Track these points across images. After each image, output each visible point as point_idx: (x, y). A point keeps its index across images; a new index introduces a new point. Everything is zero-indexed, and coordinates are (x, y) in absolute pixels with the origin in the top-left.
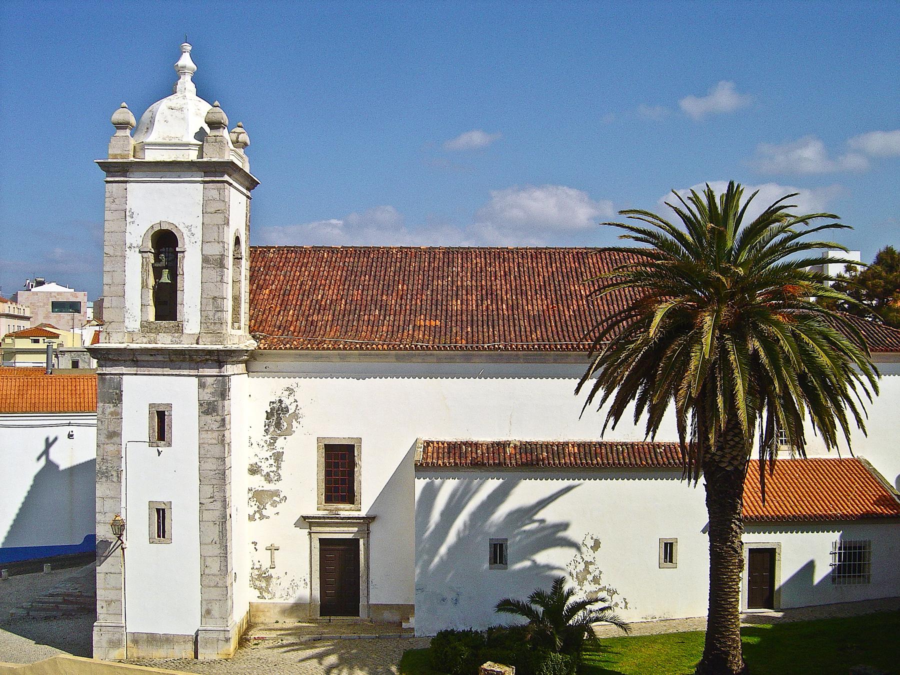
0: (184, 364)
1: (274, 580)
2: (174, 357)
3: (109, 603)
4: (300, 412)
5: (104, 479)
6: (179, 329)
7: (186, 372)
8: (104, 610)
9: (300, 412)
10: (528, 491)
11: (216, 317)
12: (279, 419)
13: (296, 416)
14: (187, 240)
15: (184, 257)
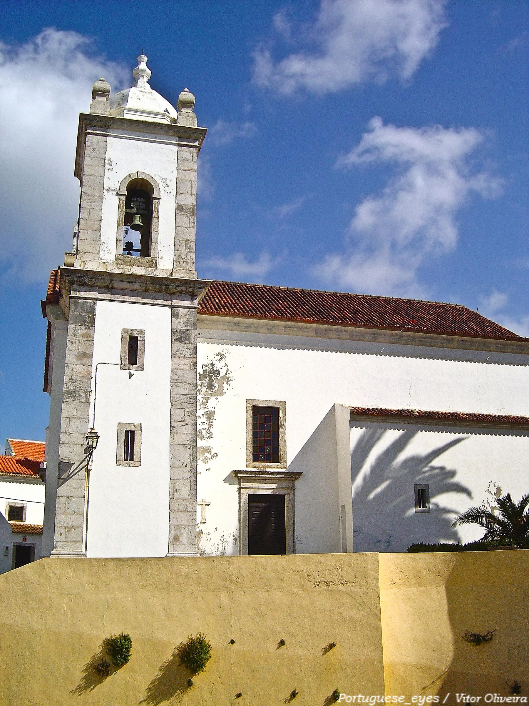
0: (158, 295)
1: (204, 536)
2: (150, 287)
3: (68, 529)
4: (231, 375)
5: (71, 399)
6: (153, 264)
7: (160, 302)
8: (63, 538)
9: (231, 375)
10: (424, 442)
11: (189, 257)
12: (211, 380)
13: (226, 378)
14: (162, 189)
15: (159, 204)
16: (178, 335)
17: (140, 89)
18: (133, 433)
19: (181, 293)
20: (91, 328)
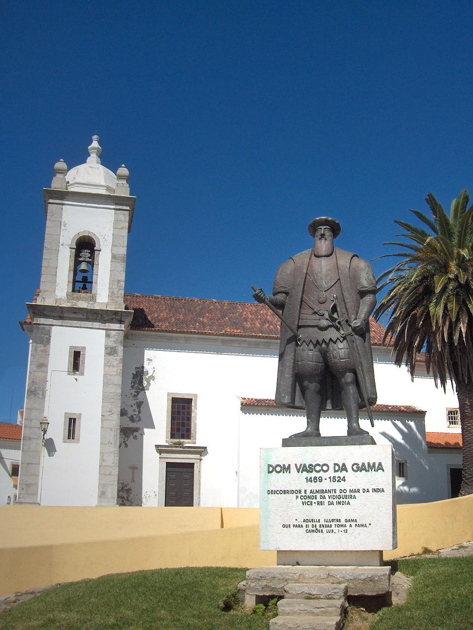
6: (93, 299)
13: (152, 377)
14: (101, 244)
16: (109, 350)
18: (75, 419)
19: (112, 320)
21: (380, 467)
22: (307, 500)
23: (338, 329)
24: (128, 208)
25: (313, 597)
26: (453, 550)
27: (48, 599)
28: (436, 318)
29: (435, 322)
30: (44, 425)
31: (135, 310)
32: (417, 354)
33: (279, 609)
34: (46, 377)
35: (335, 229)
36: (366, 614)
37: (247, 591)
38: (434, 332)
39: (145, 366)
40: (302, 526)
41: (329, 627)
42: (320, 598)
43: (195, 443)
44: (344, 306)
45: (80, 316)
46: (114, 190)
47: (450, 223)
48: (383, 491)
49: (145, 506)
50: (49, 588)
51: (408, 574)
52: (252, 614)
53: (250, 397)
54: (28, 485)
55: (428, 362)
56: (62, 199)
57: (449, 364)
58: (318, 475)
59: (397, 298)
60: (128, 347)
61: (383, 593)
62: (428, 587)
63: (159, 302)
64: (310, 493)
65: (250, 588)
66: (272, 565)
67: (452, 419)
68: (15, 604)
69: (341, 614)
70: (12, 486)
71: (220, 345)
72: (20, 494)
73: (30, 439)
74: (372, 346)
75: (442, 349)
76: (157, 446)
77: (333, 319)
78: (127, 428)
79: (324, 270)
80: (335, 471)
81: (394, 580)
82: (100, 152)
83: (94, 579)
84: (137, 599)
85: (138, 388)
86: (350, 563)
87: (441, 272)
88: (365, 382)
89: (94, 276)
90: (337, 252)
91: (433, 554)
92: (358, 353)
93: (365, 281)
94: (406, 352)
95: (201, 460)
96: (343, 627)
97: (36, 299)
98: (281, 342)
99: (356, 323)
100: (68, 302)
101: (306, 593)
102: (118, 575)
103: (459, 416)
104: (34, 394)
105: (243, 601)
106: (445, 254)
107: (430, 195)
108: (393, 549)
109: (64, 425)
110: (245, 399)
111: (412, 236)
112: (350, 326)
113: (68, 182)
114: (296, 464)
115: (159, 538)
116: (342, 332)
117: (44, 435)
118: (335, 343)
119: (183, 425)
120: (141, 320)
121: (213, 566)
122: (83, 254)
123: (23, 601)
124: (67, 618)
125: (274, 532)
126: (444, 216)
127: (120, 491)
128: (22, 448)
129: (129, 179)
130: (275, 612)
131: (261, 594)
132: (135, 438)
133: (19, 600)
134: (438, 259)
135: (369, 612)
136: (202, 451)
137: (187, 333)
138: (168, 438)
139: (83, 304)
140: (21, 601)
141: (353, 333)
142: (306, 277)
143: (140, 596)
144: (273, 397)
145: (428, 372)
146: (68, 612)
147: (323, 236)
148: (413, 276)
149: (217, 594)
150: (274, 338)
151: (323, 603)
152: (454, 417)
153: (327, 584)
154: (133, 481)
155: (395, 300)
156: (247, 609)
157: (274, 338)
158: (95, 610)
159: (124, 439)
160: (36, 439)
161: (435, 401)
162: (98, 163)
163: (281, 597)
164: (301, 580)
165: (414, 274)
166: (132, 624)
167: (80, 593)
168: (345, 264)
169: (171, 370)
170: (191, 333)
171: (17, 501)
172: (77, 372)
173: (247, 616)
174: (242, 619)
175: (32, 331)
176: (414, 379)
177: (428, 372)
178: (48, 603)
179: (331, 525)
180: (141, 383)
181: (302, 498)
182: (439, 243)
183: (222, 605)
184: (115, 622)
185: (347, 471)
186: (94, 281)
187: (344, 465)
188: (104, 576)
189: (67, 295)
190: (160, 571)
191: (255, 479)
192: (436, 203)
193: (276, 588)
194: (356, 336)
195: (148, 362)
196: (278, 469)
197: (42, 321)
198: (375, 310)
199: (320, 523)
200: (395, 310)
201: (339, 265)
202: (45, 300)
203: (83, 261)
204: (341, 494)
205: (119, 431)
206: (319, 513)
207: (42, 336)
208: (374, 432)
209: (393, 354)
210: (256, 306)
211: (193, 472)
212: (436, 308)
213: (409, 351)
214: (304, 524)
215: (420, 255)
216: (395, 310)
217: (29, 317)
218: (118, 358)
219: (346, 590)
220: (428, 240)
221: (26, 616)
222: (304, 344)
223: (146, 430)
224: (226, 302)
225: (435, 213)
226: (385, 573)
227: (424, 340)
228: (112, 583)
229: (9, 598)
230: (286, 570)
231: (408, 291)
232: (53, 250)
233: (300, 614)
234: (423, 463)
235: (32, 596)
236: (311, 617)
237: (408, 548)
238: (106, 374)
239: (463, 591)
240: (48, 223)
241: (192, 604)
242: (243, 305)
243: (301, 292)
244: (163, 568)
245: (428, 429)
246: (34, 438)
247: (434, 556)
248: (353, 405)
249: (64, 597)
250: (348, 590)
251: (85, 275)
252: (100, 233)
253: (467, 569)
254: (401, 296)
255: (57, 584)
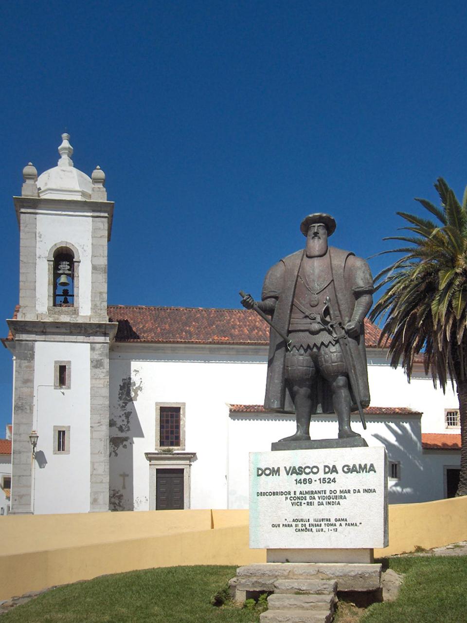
6: (76, 312)
13: (140, 388)
14: (80, 254)
16: (95, 363)
17: (62, 168)
18: (64, 432)
19: (96, 333)
20: (32, 361)
21: (372, 468)
22: (296, 501)
23: (330, 333)
24: (106, 215)
25: (302, 592)
26: (447, 549)
27: (44, 601)
28: (439, 316)
29: (437, 320)
30: (33, 439)
31: (119, 322)
32: (416, 355)
33: (269, 604)
34: (32, 392)
35: (329, 226)
36: (356, 609)
37: (238, 587)
38: (435, 332)
39: (132, 377)
40: (291, 526)
41: (319, 620)
42: (310, 593)
43: (184, 450)
44: (337, 309)
45: (63, 330)
46: (90, 195)
47: (462, 211)
48: (374, 491)
49: (136, 510)
50: (45, 590)
51: (399, 572)
52: (242, 608)
53: (239, 403)
54: (21, 497)
55: (427, 364)
56: (35, 208)
57: (450, 364)
58: (307, 477)
59: (396, 297)
60: (114, 359)
61: (374, 589)
62: (420, 584)
63: (143, 312)
64: (300, 494)
65: (240, 584)
66: (262, 563)
67: (451, 420)
68: (12, 608)
69: (330, 609)
70: (5, 497)
71: (208, 354)
72: (13, 505)
73: (20, 453)
74: (366, 349)
75: (443, 349)
76: (146, 454)
77: (325, 322)
78: (116, 438)
79: (317, 271)
80: (325, 473)
81: (385, 577)
82: (72, 152)
83: (89, 581)
84: (131, 597)
85: (125, 399)
86: (340, 561)
87: (447, 266)
88: (358, 386)
89: (75, 289)
90: (331, 251)
91: (426, 553)
92: (352, 356)
93: (361, 282)
94: (403, 353)
95: (190, 465)
96: (332, 621)
97: (16, 315)
98: (270, 349)
99: (350, 326)
100: (50, 317)
101: (296, 589)
102: (112, 575)
103: (458, 416)
104: (22, 409)
105: (234, 596)
106: (453, 246)
107: (441, 181)
108: (384, 547)
109: (54, 437)
110: (234, 405)
111: (415, 229)
112: (343, 328)
113: (39, 189)
114: (285, 467)
115: (151, 540)
116: (335, 335)
117: (34, 448)
118: (327, 346)
119: (172, 432)
120: (126, 332)
121: (204, 564)
122: (62, 266)
123: (20, 604)
124: (64, 617)
125: (263, 532)
126: (456, 203)
127: (112, 497)
128: (13, 462)
129: (105, 183)
130: (265, 606)
131: (252, 590)
132: (125, 446)
133: (16, 604)
134: (444, 252)
135: (359, 607)
136: (191, 457)
137: (174, 342)
138: (158, 446)
139: (65, 319)
140: (18, 605)
141: (347, 336)
142: (297, 279)
143: (134, 594)
144: (262, 403)
145: (427, 373)
146: (64, 612)
147: (316, 234)
148: (414, 272)
149: (208, 590)
150: (262, 344)
151: (313, 598)
152: (454, 418)
153: (317, 580)
154: (124, 487)
155: (394, 299)
156: (238, 604)
157: (262, 344)
158: (91, 609)
159: (114, 449)
160: (27, 452)
161: (433, 402)
162: (70, 165)
163: (271, 593)
164: (291, 576)
165: (415, 271)
166: (126, 620)
167: (76, 594)
168: (339, 263)
169: (158, 380)
170: (178, 342)
171: (10, 512)
172: (63, 387)
173: (238, 611)
174: (233, 614)
175: (14, 348)
176: (411, 380)
177: (427, 373)
178: (45, 605)
179: (321, 524)
180: (128, 393)
181: (291, 498)
182: (447, 234)
183: (213, 600)
184: (111, 619)
185: (337, 473)
186: (75, 294)
187: (334, 467)
188: (99, 577)
189: (49, 310)
190: (153, 571)
191: (244, 482)
192: (447, 189)
193: (266, 584)
194: (349, 339)
195: (135, 373)
196: (268, 472)
197: (24, 337)
198: (370, 311)
199: (309, 523)
200: (393, 310)
201: (333, 266)
202: (25, 316)
203: (62, 274)
204: (331, 495)
205: (108, 441)
206: (307, 512)
207: (26, 352)
208: (366, 435)
209: (389, 356)
210: (244, 313)
211: (183, 477)
212: (439, 306)
213: (406, 352)
214: (294, 524)
215: (424, 249)
216: (393, 310)
217: (10, 334)
218: (105, 371)
219: (336, 586)
220: (434, 232)
221: (23, 618)
222: (295, 348)
223: (135, 439)
224: (213, 309)
225: (445, 201)
226: (375, 570)
227: (424, 340)
228: (106, 584)
229: (6, 602)
230: (276, 567)
231: (408, 289)
232: (29, 263)
233: (290, 608)
234: (418, 464)
235: (30, 599)
236: (300, 611)
237: (401, 545)
238: (94, 387)
239: (459, 589)
240: (22, 235)
241: (184, 600)
242: (230, 312)
243: (292, 296)
244: (156, 567)
245: (424, 430)
246: (24, 452)
247: (428, 554)
248: (345, 408)
249: (60, 598)
250: (338, 586)
251: (65, 288)
252: (78, 244)
253: (463, 568)
254: (400, 294)
255: (53, 587)
